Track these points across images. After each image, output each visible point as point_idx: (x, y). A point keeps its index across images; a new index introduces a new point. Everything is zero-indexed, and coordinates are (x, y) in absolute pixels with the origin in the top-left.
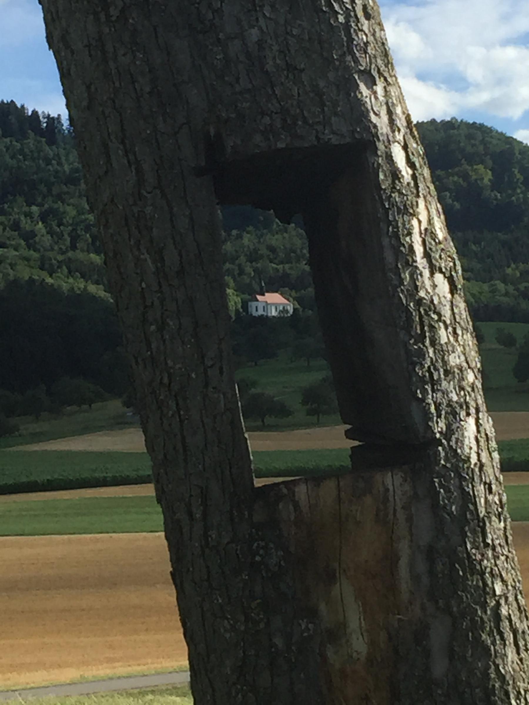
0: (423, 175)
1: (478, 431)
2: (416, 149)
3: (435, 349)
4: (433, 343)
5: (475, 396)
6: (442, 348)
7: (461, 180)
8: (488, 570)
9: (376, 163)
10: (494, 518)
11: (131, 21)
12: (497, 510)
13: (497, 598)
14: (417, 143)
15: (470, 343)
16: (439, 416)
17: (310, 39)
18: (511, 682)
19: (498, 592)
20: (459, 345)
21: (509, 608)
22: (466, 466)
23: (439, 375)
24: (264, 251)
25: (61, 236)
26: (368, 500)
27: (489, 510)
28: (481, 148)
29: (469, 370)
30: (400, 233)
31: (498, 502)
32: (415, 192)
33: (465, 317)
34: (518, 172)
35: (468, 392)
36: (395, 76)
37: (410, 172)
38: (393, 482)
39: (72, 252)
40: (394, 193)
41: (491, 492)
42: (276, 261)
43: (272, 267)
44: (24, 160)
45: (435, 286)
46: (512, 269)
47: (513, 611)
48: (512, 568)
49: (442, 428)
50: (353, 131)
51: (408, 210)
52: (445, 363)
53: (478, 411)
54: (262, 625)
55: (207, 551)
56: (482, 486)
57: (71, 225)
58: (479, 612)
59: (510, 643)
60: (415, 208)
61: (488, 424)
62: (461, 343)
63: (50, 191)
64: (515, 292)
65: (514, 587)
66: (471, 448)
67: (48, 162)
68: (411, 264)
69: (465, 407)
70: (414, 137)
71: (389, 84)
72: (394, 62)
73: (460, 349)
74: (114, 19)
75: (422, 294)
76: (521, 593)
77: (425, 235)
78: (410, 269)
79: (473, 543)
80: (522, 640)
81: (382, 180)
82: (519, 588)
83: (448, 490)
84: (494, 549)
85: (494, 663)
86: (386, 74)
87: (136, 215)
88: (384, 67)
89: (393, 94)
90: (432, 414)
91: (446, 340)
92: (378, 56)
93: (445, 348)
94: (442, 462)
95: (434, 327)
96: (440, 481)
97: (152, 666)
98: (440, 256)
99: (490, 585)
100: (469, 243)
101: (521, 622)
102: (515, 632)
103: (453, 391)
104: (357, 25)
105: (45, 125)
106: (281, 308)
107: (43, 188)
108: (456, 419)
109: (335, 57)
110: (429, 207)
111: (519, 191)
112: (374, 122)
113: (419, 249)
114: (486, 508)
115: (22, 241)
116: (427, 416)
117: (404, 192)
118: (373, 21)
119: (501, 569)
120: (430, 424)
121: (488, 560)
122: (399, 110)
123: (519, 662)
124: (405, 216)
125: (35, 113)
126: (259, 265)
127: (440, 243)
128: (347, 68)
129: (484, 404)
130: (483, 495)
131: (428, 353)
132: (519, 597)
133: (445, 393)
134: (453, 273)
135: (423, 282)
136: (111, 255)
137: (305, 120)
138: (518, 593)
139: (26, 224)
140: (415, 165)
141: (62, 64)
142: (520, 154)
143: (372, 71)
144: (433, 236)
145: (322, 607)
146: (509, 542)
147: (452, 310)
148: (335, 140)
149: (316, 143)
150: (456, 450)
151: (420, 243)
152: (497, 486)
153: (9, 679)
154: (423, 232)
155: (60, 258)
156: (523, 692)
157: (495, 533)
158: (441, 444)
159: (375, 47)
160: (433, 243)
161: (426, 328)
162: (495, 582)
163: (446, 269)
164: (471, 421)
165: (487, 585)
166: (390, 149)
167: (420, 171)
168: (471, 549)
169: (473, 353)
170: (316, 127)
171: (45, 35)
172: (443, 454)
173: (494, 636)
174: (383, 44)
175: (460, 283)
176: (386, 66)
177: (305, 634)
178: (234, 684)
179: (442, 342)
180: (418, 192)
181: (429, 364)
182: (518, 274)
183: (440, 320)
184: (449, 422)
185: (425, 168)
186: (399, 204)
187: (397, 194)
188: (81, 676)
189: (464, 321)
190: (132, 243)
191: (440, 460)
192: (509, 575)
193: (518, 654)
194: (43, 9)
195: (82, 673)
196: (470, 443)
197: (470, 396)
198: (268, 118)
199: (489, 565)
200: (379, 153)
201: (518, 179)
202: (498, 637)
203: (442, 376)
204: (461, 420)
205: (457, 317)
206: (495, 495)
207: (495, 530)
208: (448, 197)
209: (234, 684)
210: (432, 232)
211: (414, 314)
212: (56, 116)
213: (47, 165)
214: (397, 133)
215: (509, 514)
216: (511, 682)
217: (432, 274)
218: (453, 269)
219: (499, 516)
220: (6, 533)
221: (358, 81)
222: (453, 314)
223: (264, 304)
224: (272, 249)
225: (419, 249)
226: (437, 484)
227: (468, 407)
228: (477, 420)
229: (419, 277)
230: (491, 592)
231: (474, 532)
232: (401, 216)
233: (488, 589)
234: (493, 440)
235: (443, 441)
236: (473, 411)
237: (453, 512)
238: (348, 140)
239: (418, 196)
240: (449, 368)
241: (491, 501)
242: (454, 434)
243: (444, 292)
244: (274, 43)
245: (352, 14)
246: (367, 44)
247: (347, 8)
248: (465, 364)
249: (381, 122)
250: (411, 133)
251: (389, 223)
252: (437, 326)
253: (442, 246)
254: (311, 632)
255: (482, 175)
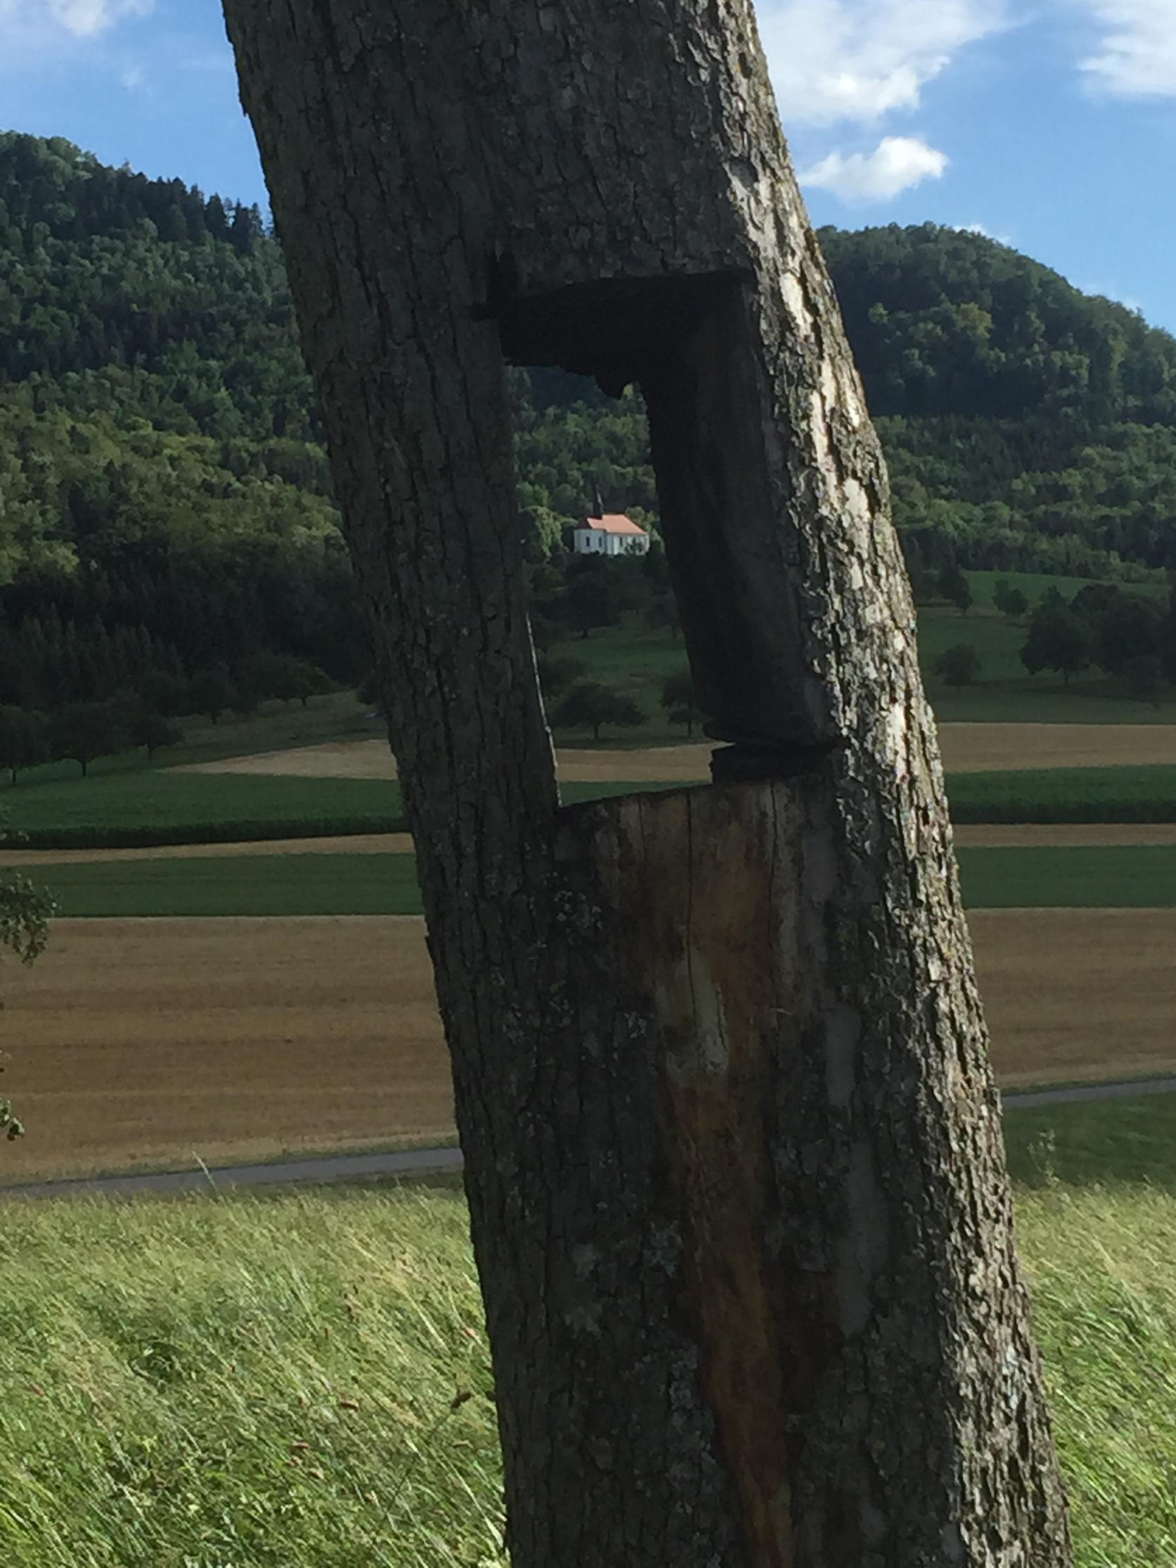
0: (830, 323)
1: (909, 727)
2: (821, 284)
3: (843, 597)
4: (841, 588)
5: (906, 673)
6: (854, 595)
7: (939, 331)
8: (919, 942)
9: (755, 305)
10: (930, 862)
11: (373, 73)
12: (936, 849)
13: (932, 985)
14: (822, 273)
15: (900, 589)
16: (847, 702)
17: (654, 106)
18: (951, 1115)
19: (934, 977)
20: (882, 592)
21: (951, 1002)
22: (887, 780)
23: (849, 637)
24: (600, 443)
25: (257, 413)
26: (734, 828)
27: (923, 850)
28: (974, 274)
29: (896, 632)
30: (792, 415)
31: (937, 838)
32: (817, 350)
33: (892, 548)
34: (1037, 317)
35: (894, 666)
36: (788, 167)
37: (810, 319)
38: (772, 802)
39: (275, 438)
40: (783, 352)
41: (926, 822)
42: (622, 461)
43: (616, 471)
44: (196, 281)
45: (844, 499)
46: (1024, 482)
47: (957, 1006)
48: (958, 940)
49: (851, 721)
50: (720, 254)
51: (807, 380)
52: (858, 619)
53: (908, 695)
54: (566, 1021)
55: (483, 905)
56: (913, 812)
57: (278, 393)
58: (904, 1007)
59: (951, 1053)
60: (815, 376)
61: (925, 717)
62: (885, 590)
63: (238, 334)
64: (1026, 520)
65: (961, 970)
66: (896, 753)
67: (238, 285)
68: (806, 462)
69: (888, 689)
70: (817, 265)
71: (779, 180)
72: (788, 147)
73: (883, 600)
74: (346, 69)
75: (824, 511)
76: (971, 980)
77: (832, 419)
78: (806, 472)
79: (896, 900)
80: (970, 1051)
81: (765, 332)
82: (968, 970)
83: (859, 817)
84: (929, 909)
85: (926, 1084)
86: (775, 164)
87: (378, 379)
88: (770, 151)
89: (784, 196)
90: (836, 698)
91: (861, 584)
92: (762, 135)
93: (859, 596)
94: (851, 773)
95: (842, 563)
96: (847, 803)
97: (404, 1138)
98: (855, 452)
99: (922, 965)
100: (951, 437)
101: (971, 1023)
102: (960, 1037)
103: (871, 664)
104: (729, 86)
105: (231, 221)
106: (630, 540)
107: (226, 328)
108: (874, 708)
109: (694, 136)
110: (839, 375)
111: (1036, 348)
112: (754, 239)
113: (821, 441)
114: (918, 847)
115: (191, 419)
116: (828, 700)
117: (799, 349)
118: (756, 80)
119: (939, 941)
120: (833, 713)
121: (919, 927)
122: (793, 222)
123: (965, 1085)
124: (800, 388)
125: (215, 199)
126: (592, 468)
127: (855, 431)
128: (712, 154)
129: (921, 687)
130: (914, 826)
131: (832, 603)
132: (968, 985)
133: (858, 666)
134: (876, 481)
135: (826, 493)
136: (338, 441)
137: (645, 237)
138: (967, 979)
139: (198, 390)
140: (818, 310)
141: (263, 136)
142: (1040, 286)
143: (753, 159)
144: (845, 420)
145: (660, 994)
146: (955, 900)
147: (872, 537)
148: (691, 268)
149: (661, 271)
150: (873, 755)
151: (823, 431)
152: (936, 813)
153: (163, 1154)
154: (828, 414)
155: (254, 447)
156: (969, 1130)
157: (931, 885)
158: (850, 746)
159: (757, 120)
160: (844, 432)
161: (829, 565)
162: (930, 960)
163: (863, 472)
164: (898, 711)
165: (918, 965)
166: (778, 282)
167: (825, 318)
168: (894, 909)
169: (903, 605)
170: (661, 246)
171: (237, 90)
172: (851, 761)
173: (927, 1045)
174: (771, 116)
175: (885, 496)
176: (775, 151)
177: (634, 1035)
178: (523, 1110)
179: (855, 587)
180: (821, 351)
181: (833, 620)
182: (1033, 491)
183: (851, 552)
184: (863, 712)
185: (835, 315)
186: (790, 369)
187: (787, 353)
188: (284, 1150)
189: (890, 554)
190: (372, 422)
191: (847, 771)
192: (953, 950)
193: (965, 1071)
194: (235, 50)
195: (285, 1146)
196: (895, 744)
197: (897, 672)
198: (587, 230)
199: (921, 934)
200: (760, 288)
201: (1038, 329)
202: (932, 1046)
203: (853, 640)
204: (882, 709)
205: (879, 547)
206: (934, 825)
207: (934, 881)
208: (916, 357)
209: (523, 1110)
210: (842, 415)
211: (811, 542)
212: (250, 207)
213: (236, 290)
214: (789, 258)
215: (957, 857)
216: (951, 1115)
217: (841, 480)
218: (874, 474)
219: (939, 859)
220: (161, 912)
221: (730, 175)
222: (873, 542)
223: (601, 534)
224: (614, 439)
225: (821, 441)
226: (841, 808)
227: (893, 689)
228: (908, 709)
229: (820, 484)
230: (923, 976)
231: (899, 884)
232: (793, 388)
233: (918, 971)
234: (934, 740)
235: (854, 741)
236: (900, 695)
237: (865, 851)
238: (712, 268)
239: (821, 358)
240: (864, 628)
241: (926, 835)
242: (870, 730)
243: (859, 509)
244: (598, 112)
245: (722, 68)
246: (744, 115)
247: (714, 59)
248: (890, 623)
249: (764, 239)
250: (813, 257)
251: (774, 399)
252: (846, 561)
253: (858, 437)
254: (643, 1032)
255: (974, 320)
